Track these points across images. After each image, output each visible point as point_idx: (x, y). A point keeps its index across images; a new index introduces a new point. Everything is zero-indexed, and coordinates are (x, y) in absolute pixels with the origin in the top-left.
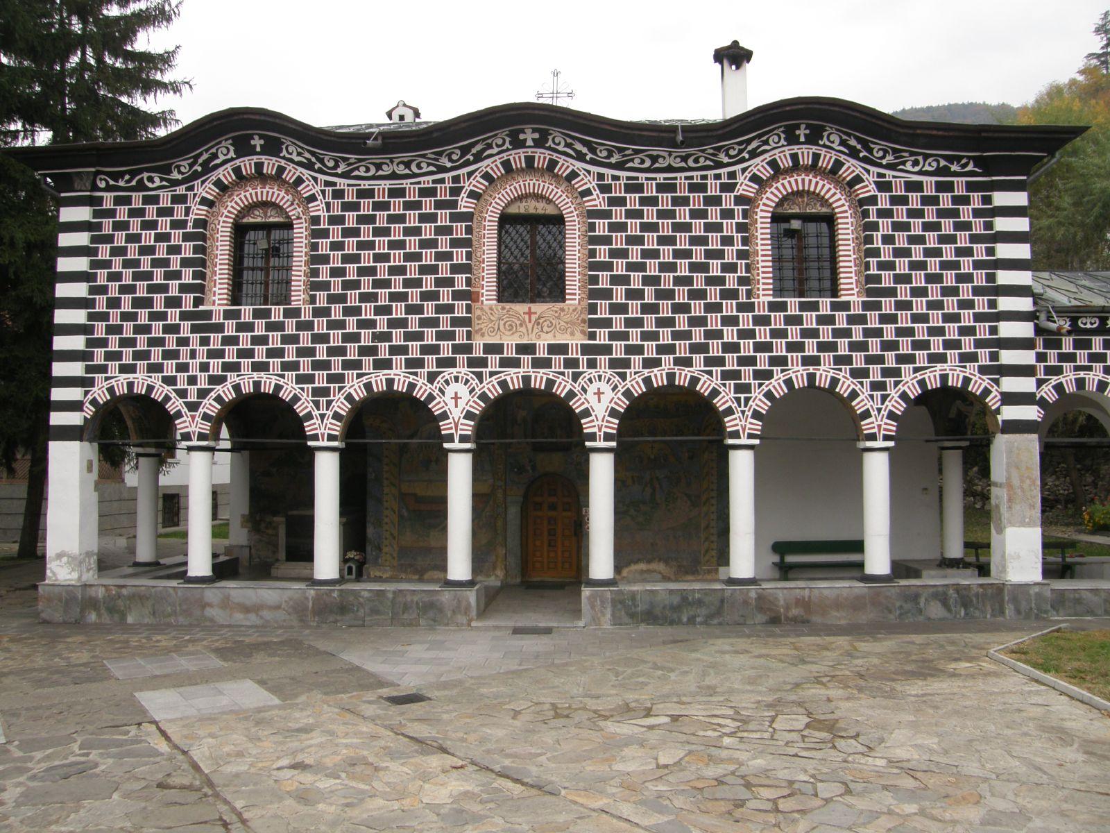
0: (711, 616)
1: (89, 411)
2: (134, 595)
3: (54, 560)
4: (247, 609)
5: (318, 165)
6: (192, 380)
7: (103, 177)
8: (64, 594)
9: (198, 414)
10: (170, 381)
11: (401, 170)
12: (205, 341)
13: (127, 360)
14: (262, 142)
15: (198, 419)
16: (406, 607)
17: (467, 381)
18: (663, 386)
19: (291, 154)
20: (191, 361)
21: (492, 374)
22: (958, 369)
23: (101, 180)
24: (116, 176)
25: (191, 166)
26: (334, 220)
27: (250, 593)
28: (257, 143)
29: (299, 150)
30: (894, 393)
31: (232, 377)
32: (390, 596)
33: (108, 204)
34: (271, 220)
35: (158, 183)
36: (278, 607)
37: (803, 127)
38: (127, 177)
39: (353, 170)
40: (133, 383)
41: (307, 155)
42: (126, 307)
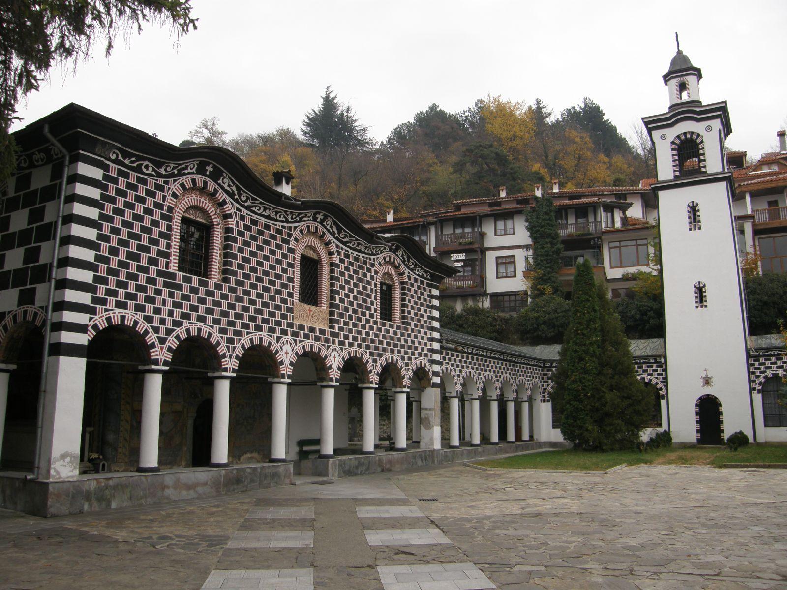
0: (366, 470)
1: (92, 333)
2: (117, 485)
3: (58, 460)
4: (189, 487)
5: (236, 197)
6: (163, 321)
7: (117, 151)
8: (72, 489)
9: (165, 346)
10: (149, 319)
11: (273, 216)
12: (171, 295)
13: (121, 298)
14: (212, 169)
15: (165, 350)
16: (266, 477)
17: (291, 344)
18: (118, 325)
19: (224, 184)
20: (163, 307)
21: (301, 341)
22: (208, 327)
23: (114, 153)
24: (126, 155)
25: (174, 168)
26: (241, 234)
27: (191, 475)
28: (209, 169)
29: (231, 183)
30: (238, 346)
31: (186, 323)
32: (259, 470)
33: (113, 173)
34: (198, 219)
35: (150, 171)
36: (206, 484)
37: (211, 165)
38: (134, 159)
39: (252, 207)
40: (125, 316)
41: (234, 188)
42: (122, 257)
